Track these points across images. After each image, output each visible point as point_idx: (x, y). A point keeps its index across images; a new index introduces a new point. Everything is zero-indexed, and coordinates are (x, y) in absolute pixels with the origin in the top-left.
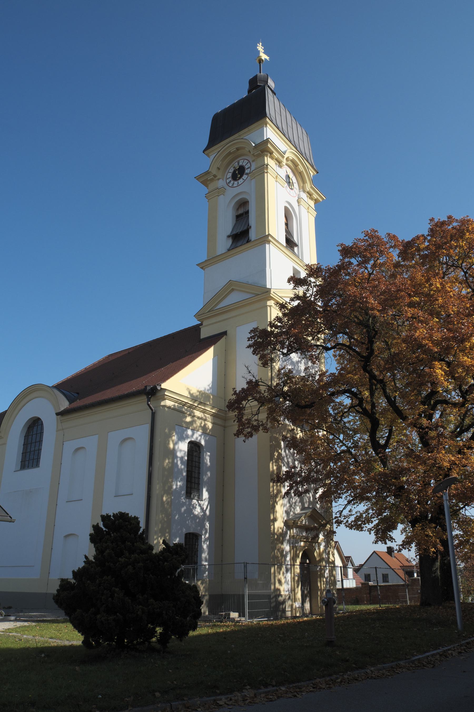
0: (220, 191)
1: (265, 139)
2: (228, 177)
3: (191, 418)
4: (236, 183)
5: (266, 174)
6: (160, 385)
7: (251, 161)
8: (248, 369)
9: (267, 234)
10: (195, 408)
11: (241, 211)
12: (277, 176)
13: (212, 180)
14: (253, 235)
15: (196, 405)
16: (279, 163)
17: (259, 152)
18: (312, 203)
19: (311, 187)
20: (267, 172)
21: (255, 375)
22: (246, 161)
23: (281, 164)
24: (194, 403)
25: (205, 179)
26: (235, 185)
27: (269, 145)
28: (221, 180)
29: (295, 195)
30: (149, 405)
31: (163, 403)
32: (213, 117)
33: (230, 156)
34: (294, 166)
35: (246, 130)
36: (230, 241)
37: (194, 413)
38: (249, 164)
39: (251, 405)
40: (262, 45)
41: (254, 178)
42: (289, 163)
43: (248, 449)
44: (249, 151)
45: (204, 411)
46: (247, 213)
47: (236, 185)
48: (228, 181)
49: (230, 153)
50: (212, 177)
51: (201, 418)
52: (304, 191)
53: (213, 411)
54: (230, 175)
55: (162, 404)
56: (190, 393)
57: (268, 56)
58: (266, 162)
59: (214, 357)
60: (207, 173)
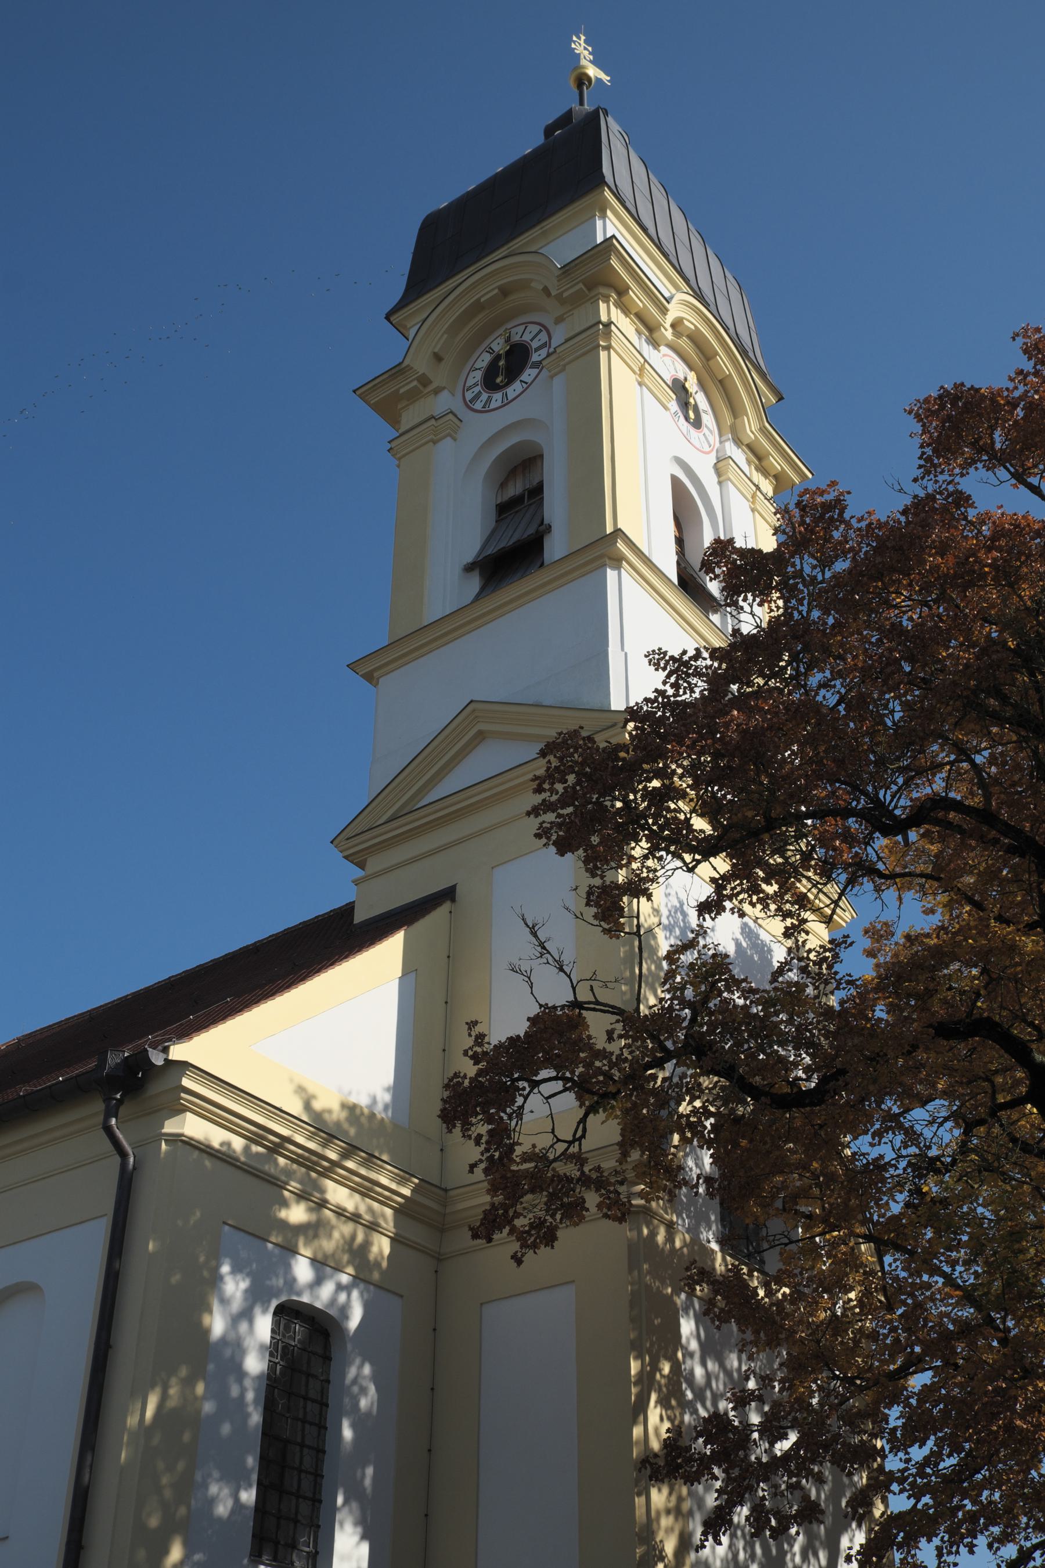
0: (443, 426)
1: (600, 239)
2: (468, 384)
3: (310, 1210)
4: (498, 396)
5: (603, 355)
6: (166, 1050)
7: (549, 324)
8: (535, 934)
9: (609, 530)
10: (329, 1170)
11: (515, 489)
12: (643, 370)
13: (413, 396)
14: (555, 547)
15: (333, 1156)
16: (650, 329)
17: (581, 285)
18: (767, 487)
19: (763, 430)
20: (608, 348)
21: (566, 959)
22: (534, 329)
23: (656, 335)
24: (324, 1146)
25: (389, 395)
26: (493, 405)
27: (614, 262)
28: (445, 395)
29: (707, 449)
30: (108, 1130)
31: (170, 1127)
32: (428, 217)
33: (480, 316)
34: (699, 353)
35: (535, 232)
36: (474, 583)
37: (323, 1191)
38: (544, 333)
39: (546, 1112)
40: (585, 41)
41: (563, 370)
42: (684, 343)
43: (536, 1309)
44: (546, 291)
45: (366, 1189)
46: (537, 491)
47: (499, 403)
48: (469, 395)
49: (478, 307)
50: (415, 383)
51: (355, 1218)
52: (738, 442)
53: (406, 1192)
54: (478, 375)
55: (165, 1130)
56: (307, 1106)
57: (607, 74)
58: (604, 318)
59: (405, 973)
60: (398, 371)
